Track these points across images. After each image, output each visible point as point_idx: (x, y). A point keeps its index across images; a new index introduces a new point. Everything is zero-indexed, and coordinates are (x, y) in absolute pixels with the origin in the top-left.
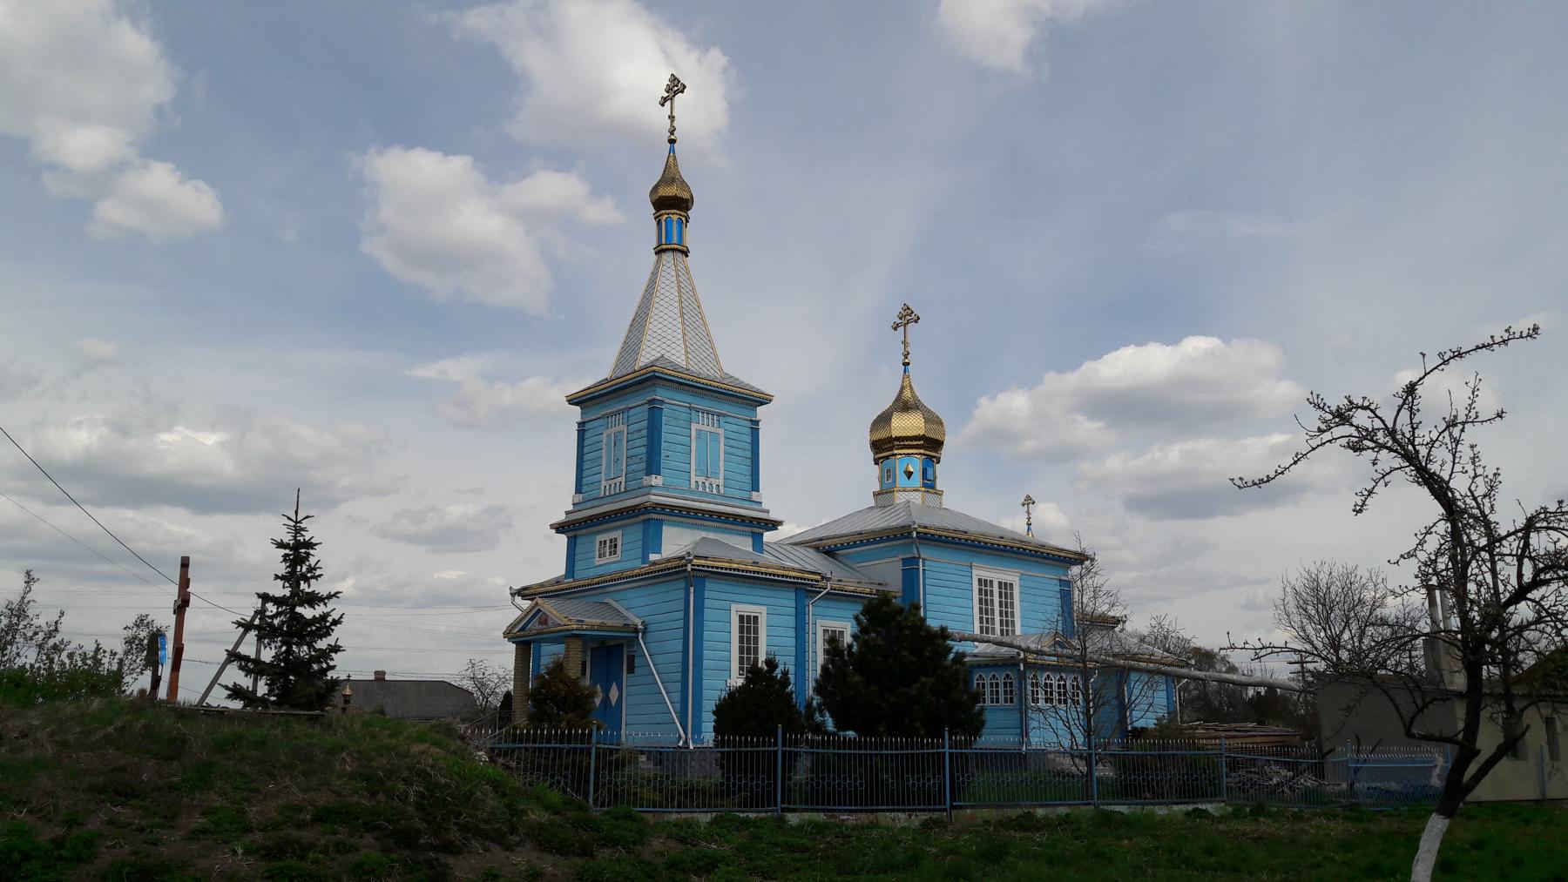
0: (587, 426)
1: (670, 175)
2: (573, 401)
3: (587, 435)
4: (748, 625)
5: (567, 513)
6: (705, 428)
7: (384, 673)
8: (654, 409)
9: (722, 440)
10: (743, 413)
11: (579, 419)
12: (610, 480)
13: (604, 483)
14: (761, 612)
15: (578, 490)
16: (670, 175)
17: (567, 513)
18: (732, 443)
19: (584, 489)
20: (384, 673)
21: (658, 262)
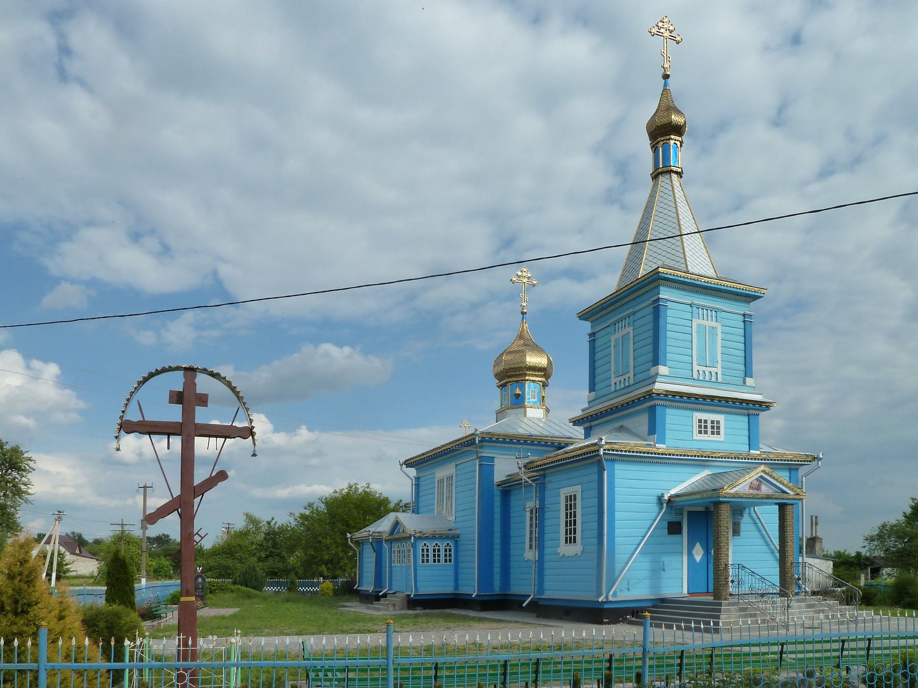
0: (597, 336)
1: (667, 106)
2: (409, 463)
3: (598, 343)
4: (571, 499)
5: (583, 410)
6: (705, 323)
7: (172, 393)
8: (657, 310)
9: (719, 334)
10: (742, 308)
11: (589, 331)
12: (616, 380)
13: (613, 380)
14: (576, 490)
15: (592, 388)
16: (667, 106)
17: (583, 410)
18: (730, 337)
19: (597, 387)
20: (172, 393)
21: (655, 186)
